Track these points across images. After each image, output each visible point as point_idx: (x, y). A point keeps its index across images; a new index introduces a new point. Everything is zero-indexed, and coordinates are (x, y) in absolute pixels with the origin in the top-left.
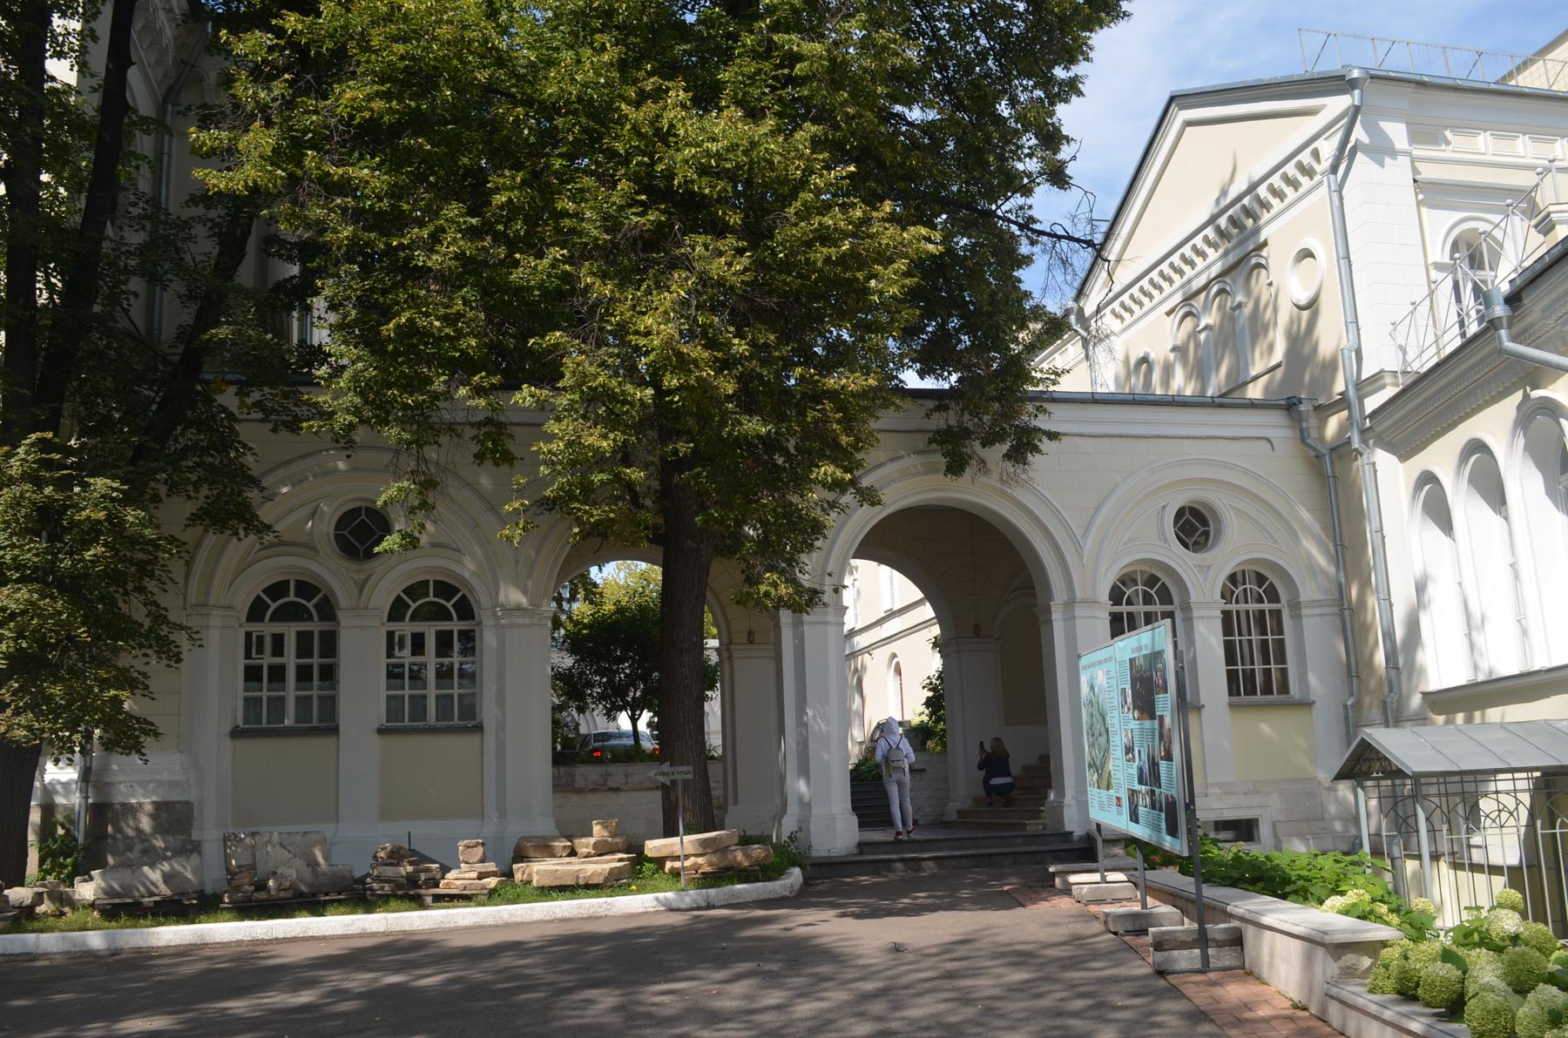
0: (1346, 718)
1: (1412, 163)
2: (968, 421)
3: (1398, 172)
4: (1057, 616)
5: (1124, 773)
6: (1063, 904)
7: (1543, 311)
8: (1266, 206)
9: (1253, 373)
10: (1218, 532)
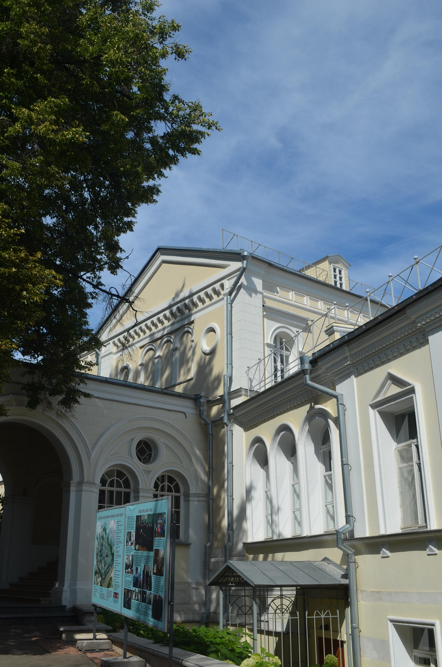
0: (205, 553)
1: (263, 298)
2: (44, 381)
3: (257, 300)
4: (73, 489)
5: (121, 579)
6: (71, 651)
7: (327, 369)
8: (195, 305)
9: (179, 381)
10: (156, 455)
